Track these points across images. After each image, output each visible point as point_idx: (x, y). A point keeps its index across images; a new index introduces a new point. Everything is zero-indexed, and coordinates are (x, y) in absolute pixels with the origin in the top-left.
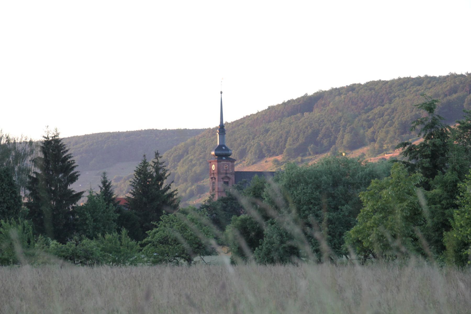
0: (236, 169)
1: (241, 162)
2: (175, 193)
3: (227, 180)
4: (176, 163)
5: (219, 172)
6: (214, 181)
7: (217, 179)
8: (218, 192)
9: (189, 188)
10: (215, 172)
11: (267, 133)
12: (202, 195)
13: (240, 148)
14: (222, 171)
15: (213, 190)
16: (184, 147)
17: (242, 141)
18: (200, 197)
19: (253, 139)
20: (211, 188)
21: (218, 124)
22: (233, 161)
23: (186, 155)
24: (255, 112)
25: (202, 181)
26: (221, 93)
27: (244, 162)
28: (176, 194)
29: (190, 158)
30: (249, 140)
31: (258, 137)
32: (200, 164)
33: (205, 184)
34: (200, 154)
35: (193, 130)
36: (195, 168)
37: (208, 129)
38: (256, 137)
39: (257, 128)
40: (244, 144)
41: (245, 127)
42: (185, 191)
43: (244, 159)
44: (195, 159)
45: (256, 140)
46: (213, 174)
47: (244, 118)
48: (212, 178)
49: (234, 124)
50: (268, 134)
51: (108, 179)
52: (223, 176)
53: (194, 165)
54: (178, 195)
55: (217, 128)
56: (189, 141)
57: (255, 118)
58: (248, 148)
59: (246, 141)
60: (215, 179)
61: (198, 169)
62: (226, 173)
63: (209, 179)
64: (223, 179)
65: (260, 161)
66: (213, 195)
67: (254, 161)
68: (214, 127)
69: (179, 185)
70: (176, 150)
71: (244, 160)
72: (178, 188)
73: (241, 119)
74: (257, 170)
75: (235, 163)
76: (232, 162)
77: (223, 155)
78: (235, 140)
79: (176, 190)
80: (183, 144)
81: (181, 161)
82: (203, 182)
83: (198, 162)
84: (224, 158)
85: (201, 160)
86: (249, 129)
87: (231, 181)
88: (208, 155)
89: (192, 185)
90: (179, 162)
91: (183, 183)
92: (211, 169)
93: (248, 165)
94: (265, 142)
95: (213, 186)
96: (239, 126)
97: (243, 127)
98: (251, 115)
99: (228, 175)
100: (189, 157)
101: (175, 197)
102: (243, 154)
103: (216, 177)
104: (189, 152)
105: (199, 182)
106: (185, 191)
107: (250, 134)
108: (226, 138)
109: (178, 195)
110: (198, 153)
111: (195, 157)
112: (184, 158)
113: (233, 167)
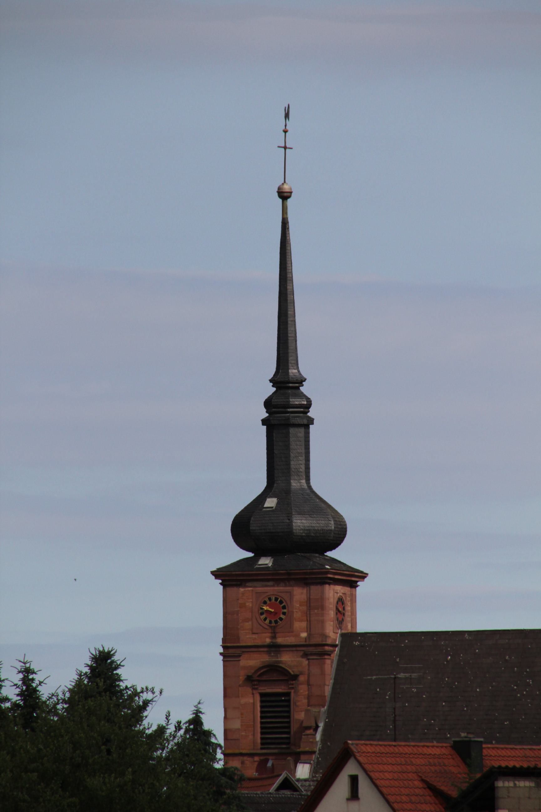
99: (287, 659)
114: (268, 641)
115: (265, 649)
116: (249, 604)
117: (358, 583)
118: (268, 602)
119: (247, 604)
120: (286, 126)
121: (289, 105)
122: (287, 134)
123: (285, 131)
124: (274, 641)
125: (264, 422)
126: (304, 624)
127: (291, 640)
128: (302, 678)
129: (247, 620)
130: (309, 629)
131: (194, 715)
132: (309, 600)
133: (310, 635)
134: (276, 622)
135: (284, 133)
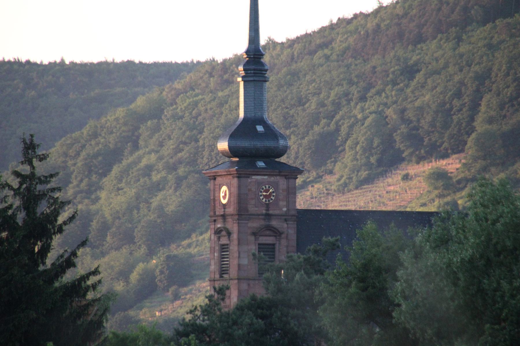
99: (274, 223)
114: (264, 212)
115: (263, 217)
117: (298, 176)
124: (268, 212)
125: (63, 61)
126: (285, 203)
127: (277, 212)
129: (252, 199)
130: (287, 206)
131: (18, 198)
132: (288, 188)
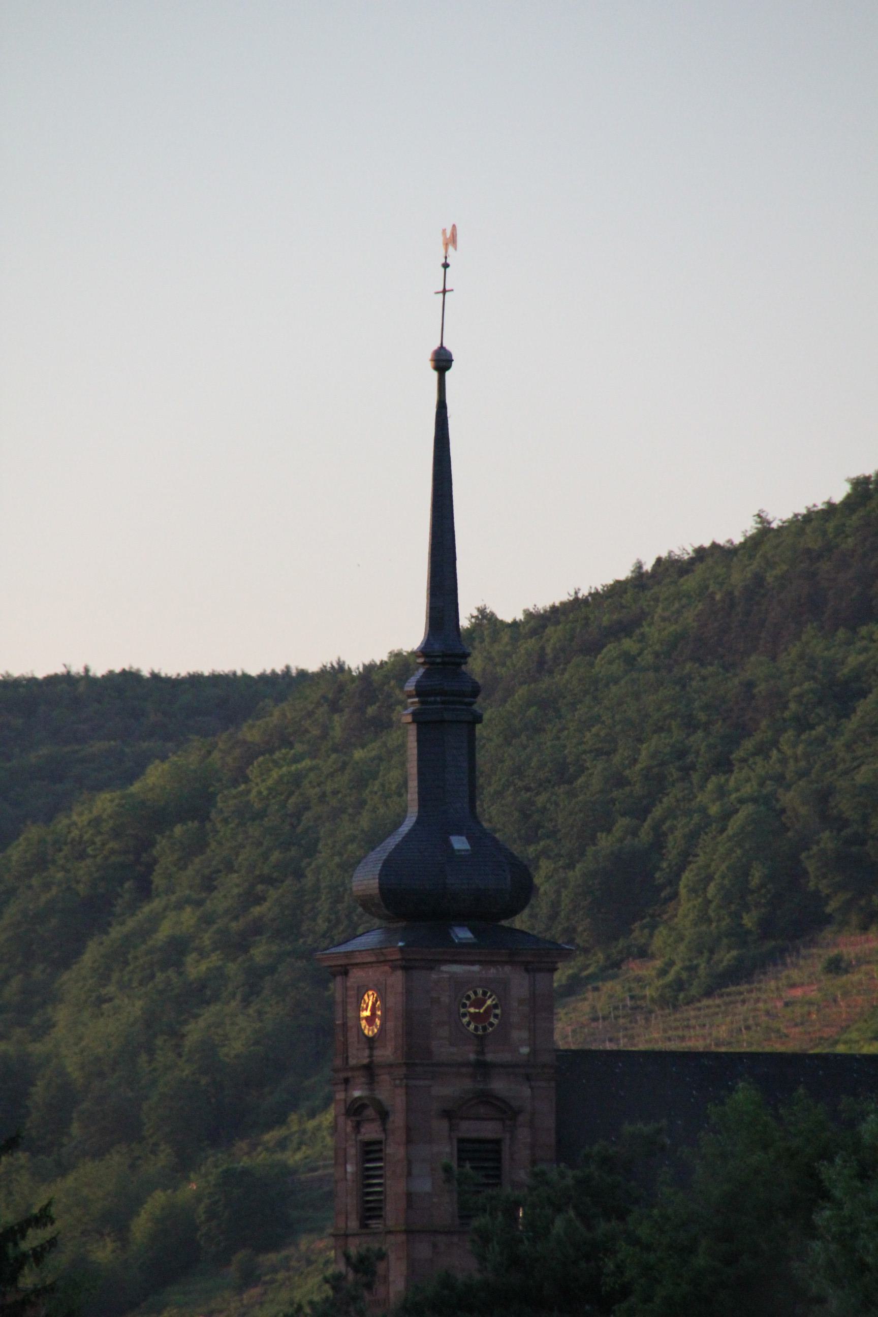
0: (570, 1028)
1: (614, 966)
2: (34, 1238)
3: (488, 1129)
4: (38, 972)
5: (416, 1059)
6: (371, 1131)
7: (398, 1120)
8: (409, 1232)
9: (159, 1198)
10: (386, 1053)
11: (846, 712)
12: (273, 1258)
13: (605, 842)
14: (443, 1049)
15: (370, 1211)
16: (117, 833)
17: (621, 781)
18: (249, 1278)
19: (723, 765)
20: (349, 1201)
21: (409, 633)
22: (540, 957)
23: (133, 908)
24: (734, 530)
25: (270, 1137)
26: (442, 362)
27: (635, 968)
28: (39, 1255)
29: (165, 931)
30: (687, 770)
31: (762, 750)
32: (255, 978)
33: (293, 1158)
34: (252, 898)
35: (195, 680)
36: (209, 1014)
37: (323, 673)
38: (749, 744)
39: (755, 667)
40: (641, 812)
41: (648, 658)
42: (116, 1222)
43: (638, 935)
44: (207, 939)
45: (744, 782)
46: (370, 1070)
47: (640, 580)
48: (355, 1110)
49: (554, 635)
50: (852, 724)
51: (770, 518)
52: (449, 1089)
53: (200, 994)
54: (60, 1260)
55: (399, 664)
56: (155, 777)
57: (738, 578)
58: (674, 843)
59: (657, 783)
60: (384, 1115)
61: (234, 1029)
62: (482, 1068)
63: (327, 1118)
64: (447, 1114)
65: (773, 959)
66: (366, 1266)
67: (727, 957)
68: (380, 655)
69: (63, 1169)
70: (40, 862)
71: (643, 953)
72: (57, 1192)
73: (618, 589)
74: (747, 1044)
75: (561, 976)
76: (529, 968)
77: (450, 904)
78: (565, 773)
79: (43, 1218)
80: (105, 802)
81: (92, 953)
82: (282, 1145)
83: (232, 968)
84: (463, 934)
85: (260, 952)
86: (683, 682)
87: (524, 1135)
88: (324, 905)
89: (184, 1165)
90: (66, 962)
91: (99, 1154)
92: (349, 1026)
93: (675, 996)
94: (823, 797)
95: (366, 1176)
96: (593, 648)
97: (630, 660)
98: (701, 553)
99: (499, 1085)
100: (155, 921)
101: (28, 1280)
102: (630, 895)
103: (390, 1093)
104: (158, 880)
105: (242, 1145)
106: (116, 1222)
107: (691, 725)
108: (482, 758)
109: (60, 1260)
110: (232, 885)
111: (207, 920)
112: (116, 932)
113: (541, 1007)
114: (472, 1057)
116: (445, 999)
118: (468, 1002)
119: (442, 999)
120: (446, 258)
121: (454, 226)
122: (448, 270)
123: (446, 266)
128: (521, 1119)
133: (534, 1052)
134: (484, 1029)
135: (443, 270)
